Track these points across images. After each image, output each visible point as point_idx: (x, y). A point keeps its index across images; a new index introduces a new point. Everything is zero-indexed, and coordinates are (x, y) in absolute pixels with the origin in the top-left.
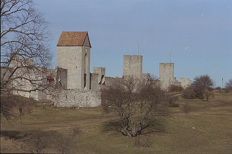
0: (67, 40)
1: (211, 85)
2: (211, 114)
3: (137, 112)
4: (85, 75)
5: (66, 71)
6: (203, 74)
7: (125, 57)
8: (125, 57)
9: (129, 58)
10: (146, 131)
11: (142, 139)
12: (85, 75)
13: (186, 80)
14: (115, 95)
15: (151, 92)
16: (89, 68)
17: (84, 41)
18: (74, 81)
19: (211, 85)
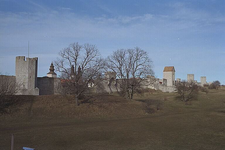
0: (167, 69)
1: (220, 84)
2: (76, 68)
3: (187, 93)
4: (173, 81)
5: (166, 80)
6: (215, 80)
7: (188, 75)
8: (188, 75)
9: (189, 75)
10: (190, 99)
11: (188, 102)
12: (173, 81)
13: (210, 81)
14: (180, 86)
15: (194, 87)
16: (175, 79)
17: (172, 70)
18: (170, 83)
19: (220, 84)
